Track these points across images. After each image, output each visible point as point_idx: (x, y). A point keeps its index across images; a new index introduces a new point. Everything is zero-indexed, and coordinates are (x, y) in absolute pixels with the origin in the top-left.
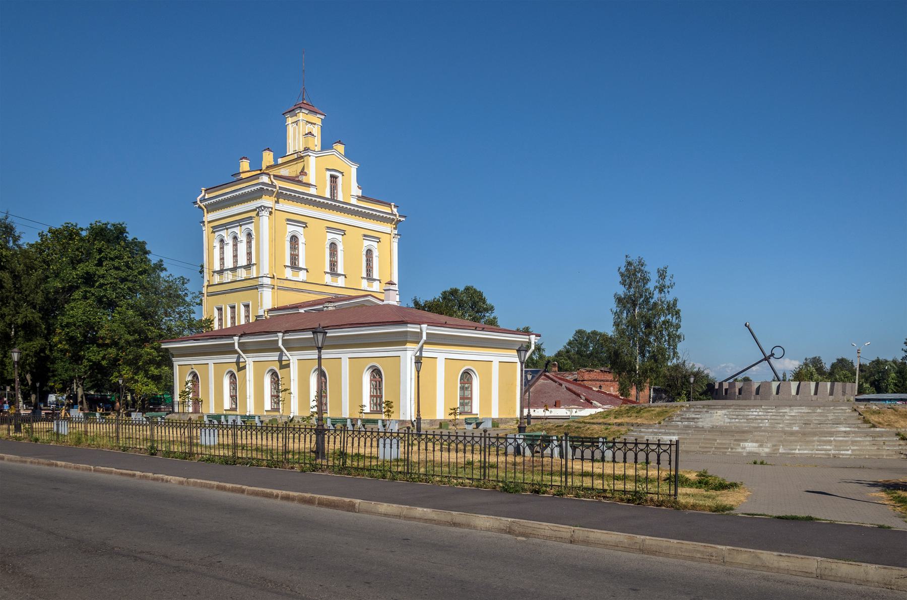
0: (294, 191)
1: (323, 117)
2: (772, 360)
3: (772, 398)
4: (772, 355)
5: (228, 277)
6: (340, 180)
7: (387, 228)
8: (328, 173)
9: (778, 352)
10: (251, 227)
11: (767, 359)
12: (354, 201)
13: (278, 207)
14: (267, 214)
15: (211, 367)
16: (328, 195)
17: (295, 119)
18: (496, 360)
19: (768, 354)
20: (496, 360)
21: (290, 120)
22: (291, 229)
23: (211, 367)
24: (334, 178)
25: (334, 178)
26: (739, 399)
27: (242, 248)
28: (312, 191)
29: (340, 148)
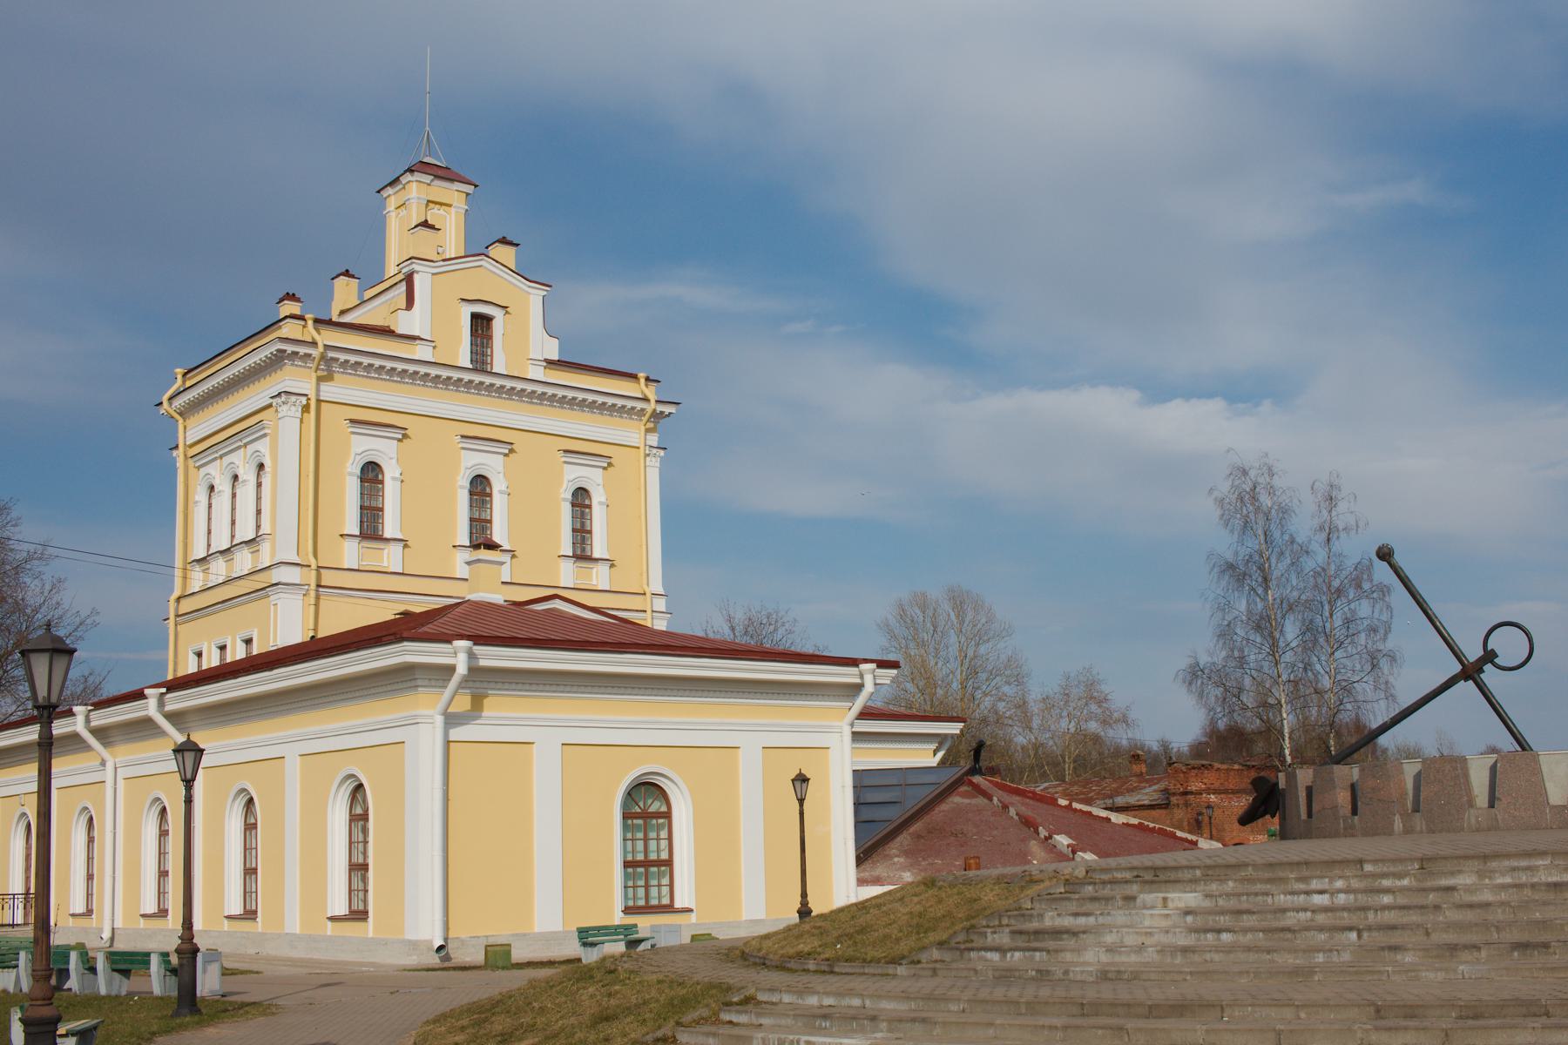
0: (378, 351)
1: (469, 189)
2: (1489, 675)
3: (1471, 817)
4: (1489, 656)
5: (219, 569)
6: (498, 327)
7: (632, 433)
8: (466, 311)
9: (1509, 646)
10: (263, 447)
11: (1470, 672)
12: (538, 373)
13: (329, 391)
14: (296, 412)
15: (293, 768)
16: (464, 359)
17: (402, 197)
18: (292, 753)
19: (1473, 653)
20: (292, 753)
21: (392, 203)
22: (575, 474)
23: (293, 768)
24: (481, 323)
25: (481, 323)
26: (1350, 832)
27: (247, 492)
28: (422, 352)
29: (506, 254)
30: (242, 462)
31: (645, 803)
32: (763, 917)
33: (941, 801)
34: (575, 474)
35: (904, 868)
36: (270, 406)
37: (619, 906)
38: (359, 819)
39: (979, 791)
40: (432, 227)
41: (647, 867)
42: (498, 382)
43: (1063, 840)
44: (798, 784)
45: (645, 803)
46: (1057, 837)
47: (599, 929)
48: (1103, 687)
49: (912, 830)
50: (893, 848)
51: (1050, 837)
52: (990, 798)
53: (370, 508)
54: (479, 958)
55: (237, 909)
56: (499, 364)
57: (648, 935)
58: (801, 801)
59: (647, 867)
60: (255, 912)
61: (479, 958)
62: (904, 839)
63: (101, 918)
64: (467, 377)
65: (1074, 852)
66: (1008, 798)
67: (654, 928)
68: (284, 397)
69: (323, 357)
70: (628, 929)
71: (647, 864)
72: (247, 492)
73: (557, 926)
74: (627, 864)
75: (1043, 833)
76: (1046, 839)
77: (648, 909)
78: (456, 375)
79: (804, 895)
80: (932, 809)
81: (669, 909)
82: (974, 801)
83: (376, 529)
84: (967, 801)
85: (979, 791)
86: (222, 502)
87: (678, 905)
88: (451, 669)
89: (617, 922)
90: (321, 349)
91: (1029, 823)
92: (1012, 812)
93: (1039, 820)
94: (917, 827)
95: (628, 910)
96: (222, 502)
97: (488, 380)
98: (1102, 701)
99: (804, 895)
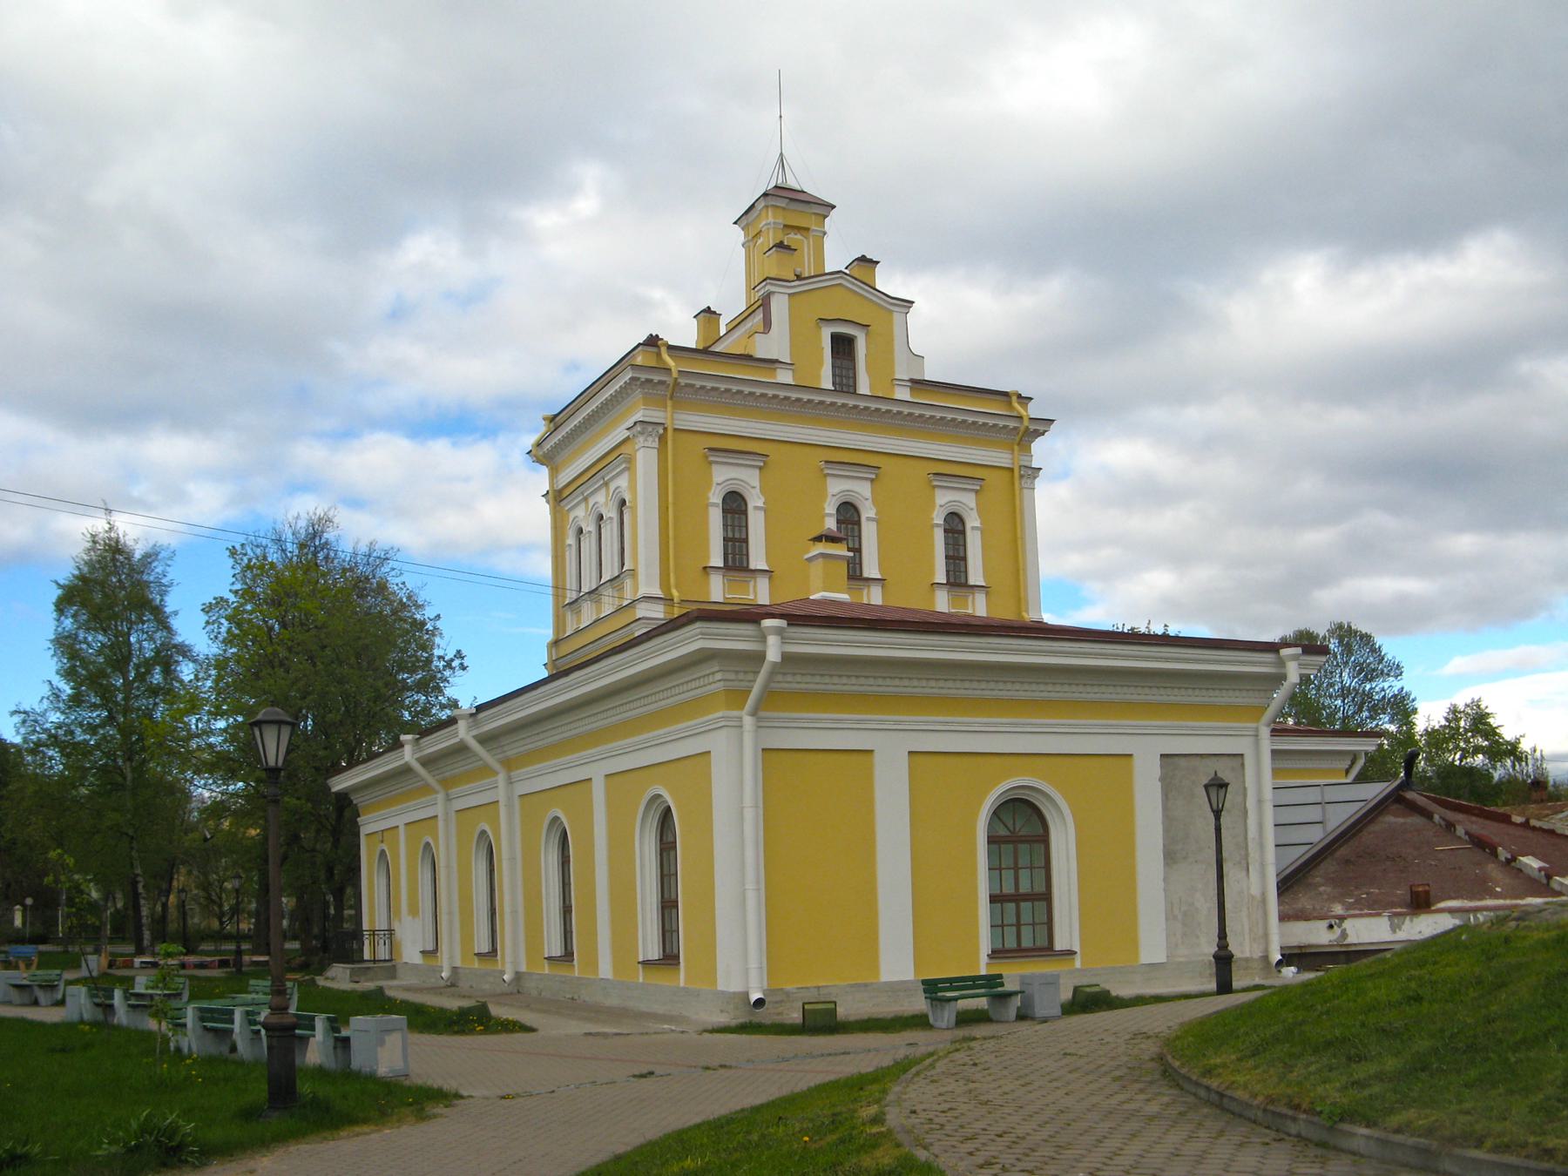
8: (826, 334)
10: (622, 482)
16: (827, 383)
24: (843, 347)
25: (843, 347)
27: (610, 532)
28: (784, 377)
30: (602, 501)
31: (1020, 827)
32: (1163, 959)
33: (1371, 821)
34: (944, 499)
35: (1333, 899)
36: (628, 439)
37: (985, 948)
38: (667, 847)
39: (1414, 808)
40: (788, 248)
41: (1023, 904)
42: (862, 404)
43: (1532, 863)
44: (1213, 792)
45: (1020, 827)
46: (1524, 859)
47: (950, 980)
48: (1491, 720)
49: (1338, 854)
50: (1317, 877)
51: (1514, 859)
52: (1429, 815)
53: (733, 540)
54: (795, 1016)
55: (654, 953)
56: (864, 387)
57: (1017, 988)
58: (1217, 814)
59: (1023, 904)
60: (677, 957)
61: (795, 1016)
62: (1329, 866)
63: (593, 963)
64: (828, 400)
65: (1549, 877)
66: (1452, 816)
67: (1023, 980)
68: (639, 428)
69: (676, 383)
70: (992, 981)
71: (1017, 898)
72: (610, 532)
73: (909, 975)
74: (994, 899)
75: (1503, 854)
76: (1508, 861)
77: (1020, 952)
78: (817, 398)
79: (1222, 935)
80: (1360, 830)
81: (1047, 950)
82: (1409, 820)
83: (741, 561)
84: (1401, 820)
85: (1414, 808)
86: (589, 545)
87: (1058, 946)
88: (760, 657)
89: (983, 972)
90: (675, 375)
91: (1482, 845)
92: (1460, 831)
93: (1496, 839)
94: (1343, 852)
95: (996, 954)
96: (589, 545)
97: (851, 402)
98: (1491, 733)
99: (1222, 935)
